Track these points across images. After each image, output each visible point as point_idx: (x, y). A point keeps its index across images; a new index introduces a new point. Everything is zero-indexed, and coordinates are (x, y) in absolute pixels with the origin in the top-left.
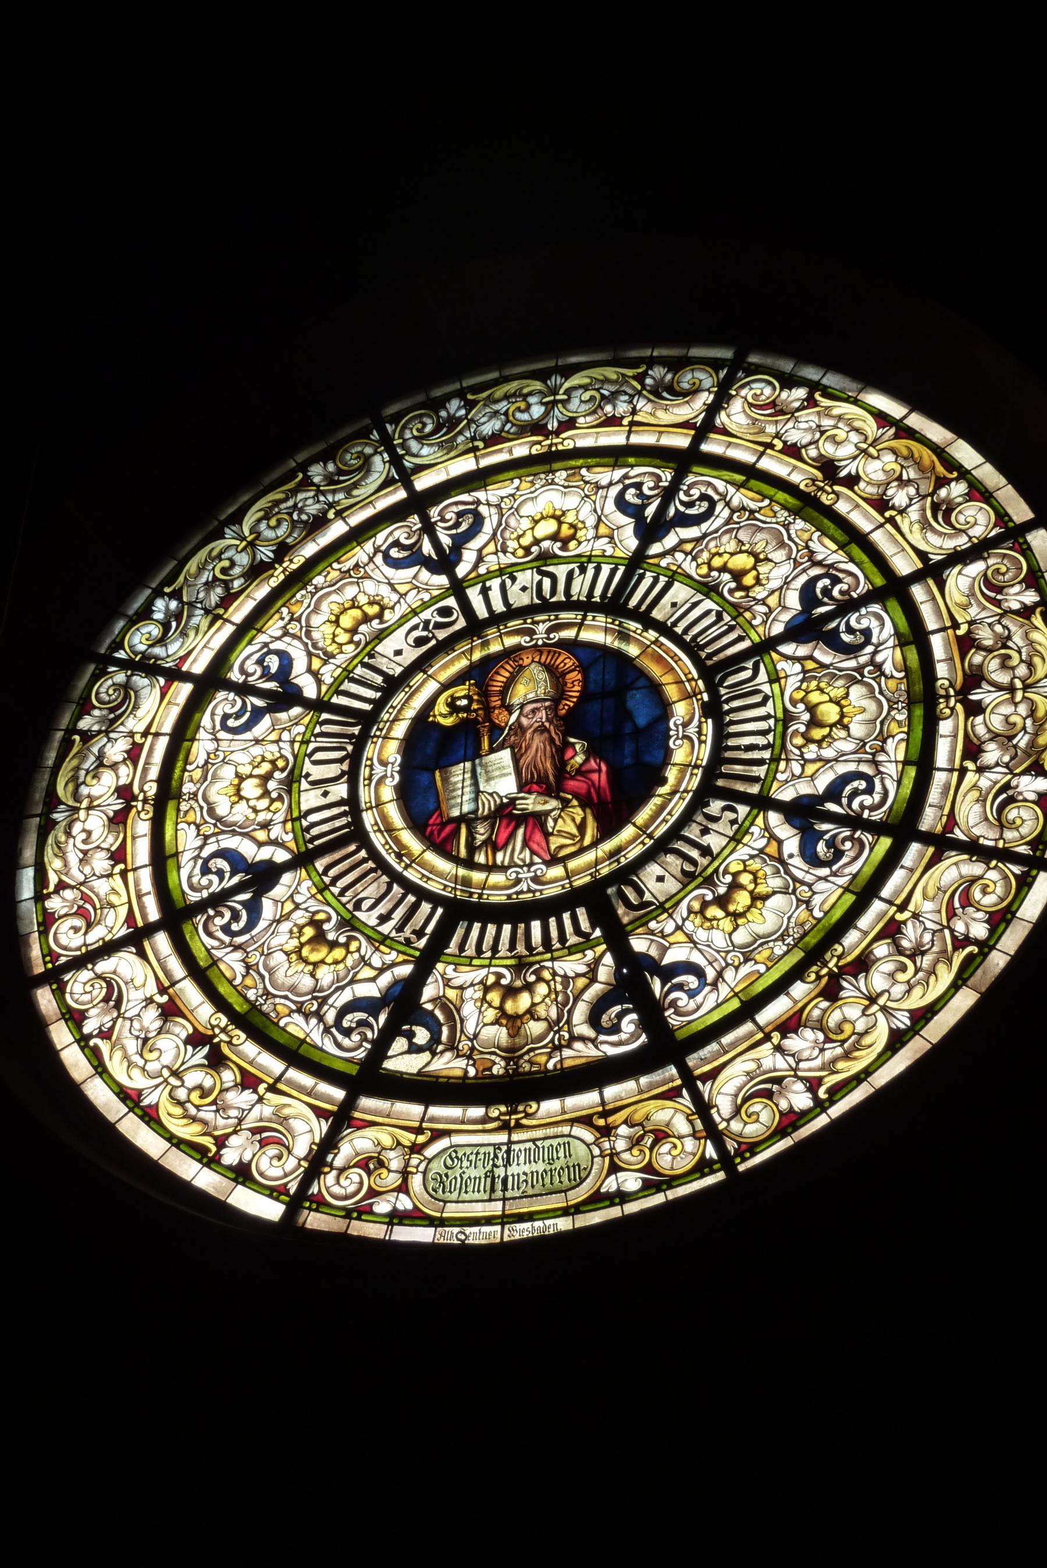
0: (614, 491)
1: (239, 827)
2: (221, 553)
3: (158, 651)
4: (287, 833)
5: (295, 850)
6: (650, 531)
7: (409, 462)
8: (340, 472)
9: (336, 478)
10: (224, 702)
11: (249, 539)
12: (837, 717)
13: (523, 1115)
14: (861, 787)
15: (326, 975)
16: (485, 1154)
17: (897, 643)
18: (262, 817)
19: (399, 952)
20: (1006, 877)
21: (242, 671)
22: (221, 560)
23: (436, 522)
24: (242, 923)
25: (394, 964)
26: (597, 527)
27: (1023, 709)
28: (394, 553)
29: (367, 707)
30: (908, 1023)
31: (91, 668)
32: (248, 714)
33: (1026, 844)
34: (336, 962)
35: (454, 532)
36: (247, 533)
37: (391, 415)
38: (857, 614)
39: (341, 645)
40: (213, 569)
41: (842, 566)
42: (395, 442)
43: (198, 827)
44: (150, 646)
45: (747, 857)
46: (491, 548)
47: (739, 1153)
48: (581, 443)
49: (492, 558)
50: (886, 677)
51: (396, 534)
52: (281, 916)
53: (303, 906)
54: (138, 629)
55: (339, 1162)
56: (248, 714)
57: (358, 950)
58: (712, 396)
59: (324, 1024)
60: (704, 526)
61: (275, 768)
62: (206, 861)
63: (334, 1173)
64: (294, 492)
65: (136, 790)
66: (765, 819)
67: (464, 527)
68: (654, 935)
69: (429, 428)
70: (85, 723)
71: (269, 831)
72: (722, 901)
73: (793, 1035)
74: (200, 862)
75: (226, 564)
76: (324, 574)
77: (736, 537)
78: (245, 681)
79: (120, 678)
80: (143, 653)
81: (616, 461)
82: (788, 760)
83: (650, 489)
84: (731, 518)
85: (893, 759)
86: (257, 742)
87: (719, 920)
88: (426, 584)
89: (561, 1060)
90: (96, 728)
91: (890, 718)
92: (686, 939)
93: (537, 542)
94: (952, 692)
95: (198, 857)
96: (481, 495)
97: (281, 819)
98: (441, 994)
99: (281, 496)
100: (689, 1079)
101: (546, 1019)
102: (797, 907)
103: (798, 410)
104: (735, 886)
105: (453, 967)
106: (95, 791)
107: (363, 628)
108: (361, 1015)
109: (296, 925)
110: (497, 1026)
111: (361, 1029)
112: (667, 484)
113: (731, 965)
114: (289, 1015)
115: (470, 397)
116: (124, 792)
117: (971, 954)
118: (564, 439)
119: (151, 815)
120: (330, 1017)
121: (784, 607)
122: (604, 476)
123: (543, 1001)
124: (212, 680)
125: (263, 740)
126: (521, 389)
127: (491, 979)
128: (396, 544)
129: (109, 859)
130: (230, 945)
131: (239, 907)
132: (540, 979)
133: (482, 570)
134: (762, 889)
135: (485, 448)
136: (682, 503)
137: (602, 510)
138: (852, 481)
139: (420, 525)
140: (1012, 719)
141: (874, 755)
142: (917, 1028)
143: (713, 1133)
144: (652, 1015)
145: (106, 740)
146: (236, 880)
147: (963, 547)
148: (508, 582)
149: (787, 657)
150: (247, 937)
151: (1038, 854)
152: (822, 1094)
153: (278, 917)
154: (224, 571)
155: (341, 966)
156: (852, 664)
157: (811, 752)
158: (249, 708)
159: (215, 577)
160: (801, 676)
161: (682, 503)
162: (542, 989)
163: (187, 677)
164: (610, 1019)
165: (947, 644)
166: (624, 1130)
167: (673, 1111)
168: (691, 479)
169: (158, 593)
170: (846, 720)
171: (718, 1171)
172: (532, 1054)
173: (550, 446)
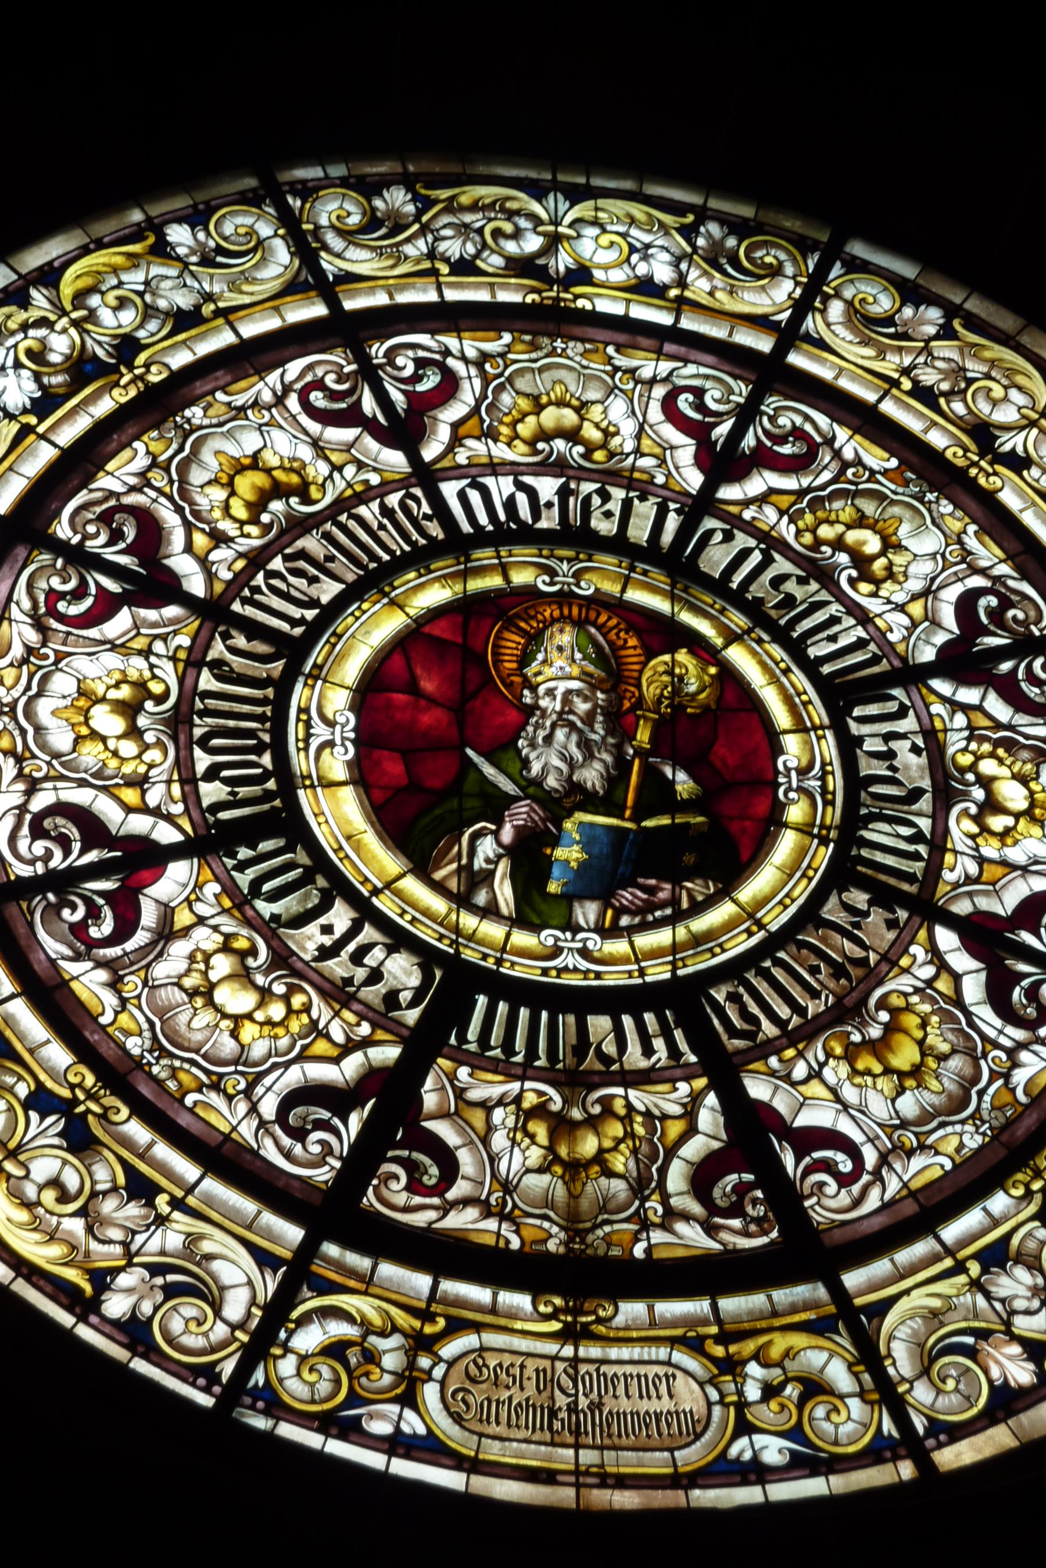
0: (977, 581)
2: (518, 213)
3: (335, 242)
4: (914, 957)
7: (812, 323)
9: (723, 261)
10: (331, 364)
11: (560, 229)
12: (906, 1067)
13: (969, 454)
14: (320, 395)
15: (91, 754)
16: (537, 1371)
17: (101, 474)
18: (227, 526)
19: (927, 706)
21: (391, 354)
22: (508, 219)
23: (340, 1158)
24: (75, 610)
25: (944, 700)
26: (914, 598)
28: (684, 402)
29: (466, 528)
30: (551, 197)
31: (251, 182)
32: (817, 1155)
33: (928, 1417)
35: (769, 444)
36: (567, 220)
37: (855, 258)
39: (517, 436)
40: (490, 220)
41: (27, 604)
43: (154, 464)
44: (332, 226)
45: (643, 1109)
47: (256, 1393)
49: (770, 514)
51: (401, 1199)
52: (123, 645)
53: (153, 659)
56: (817, 1155)
57: (965, 750)
59: (27, 802)
60: (1021, 719)
65: (141, 359)
67: (786, 449)
69: (355, 220)
71: (216, 547)
72: (562, 1127)
74: (112, 503)
75: (508, 227)
76: (588, 346)
77: (74, 751)
78: (380, 366)
79: (922, 1393)
80: (318, 228)
81: (1017, 555)
82: (800, 1054)
85: (906, 1178)
86: (315, 443)
87: (534, 1143)
88: (677, 468)
90: (181, 251)
91: (958, 1128)
95: (118, 495)
97: (241, 549)
98: (172, 904)
101: (242, 1046)
102: (627, 1220)
105: (889, 635)
106: (106, 316)
107: (560, 444)
108: (74, 833)
109: (123, 672)
110: (186, 999)
112: (1037, 633)
113: (634, 379)
115: (956, 324)
116: (127, 346)
118: (995, 474)
120: (41, 801)
121: (136, 626)
122: (987, 553)
123: (838, 522)
125: (322, 449)
126: (20, 1226)
127: (241, 944)
128: (414, 1186)
129: (31, 399)
131: (93, 590)
132: (286, 998)
133: (748, 515)
134: (524, 404)
135: (909, 393)
138: (40, 1101)
142: (549, 185)
144: (786, 1200)
146: (124, 560)
151: (930, 1443)
152: (690, 218)
153: (118, 642)
154: (497, 233)
155: (113, 763)
157: (835, 1072)
158: (807, 1160)
159: (480, 231)
161: (1029, 668)
162: (826, 532)
164: (304, 1119)
166: (753, 1369)
168: (322, 1175)
169: (408, 182)
172: (186, 1066)
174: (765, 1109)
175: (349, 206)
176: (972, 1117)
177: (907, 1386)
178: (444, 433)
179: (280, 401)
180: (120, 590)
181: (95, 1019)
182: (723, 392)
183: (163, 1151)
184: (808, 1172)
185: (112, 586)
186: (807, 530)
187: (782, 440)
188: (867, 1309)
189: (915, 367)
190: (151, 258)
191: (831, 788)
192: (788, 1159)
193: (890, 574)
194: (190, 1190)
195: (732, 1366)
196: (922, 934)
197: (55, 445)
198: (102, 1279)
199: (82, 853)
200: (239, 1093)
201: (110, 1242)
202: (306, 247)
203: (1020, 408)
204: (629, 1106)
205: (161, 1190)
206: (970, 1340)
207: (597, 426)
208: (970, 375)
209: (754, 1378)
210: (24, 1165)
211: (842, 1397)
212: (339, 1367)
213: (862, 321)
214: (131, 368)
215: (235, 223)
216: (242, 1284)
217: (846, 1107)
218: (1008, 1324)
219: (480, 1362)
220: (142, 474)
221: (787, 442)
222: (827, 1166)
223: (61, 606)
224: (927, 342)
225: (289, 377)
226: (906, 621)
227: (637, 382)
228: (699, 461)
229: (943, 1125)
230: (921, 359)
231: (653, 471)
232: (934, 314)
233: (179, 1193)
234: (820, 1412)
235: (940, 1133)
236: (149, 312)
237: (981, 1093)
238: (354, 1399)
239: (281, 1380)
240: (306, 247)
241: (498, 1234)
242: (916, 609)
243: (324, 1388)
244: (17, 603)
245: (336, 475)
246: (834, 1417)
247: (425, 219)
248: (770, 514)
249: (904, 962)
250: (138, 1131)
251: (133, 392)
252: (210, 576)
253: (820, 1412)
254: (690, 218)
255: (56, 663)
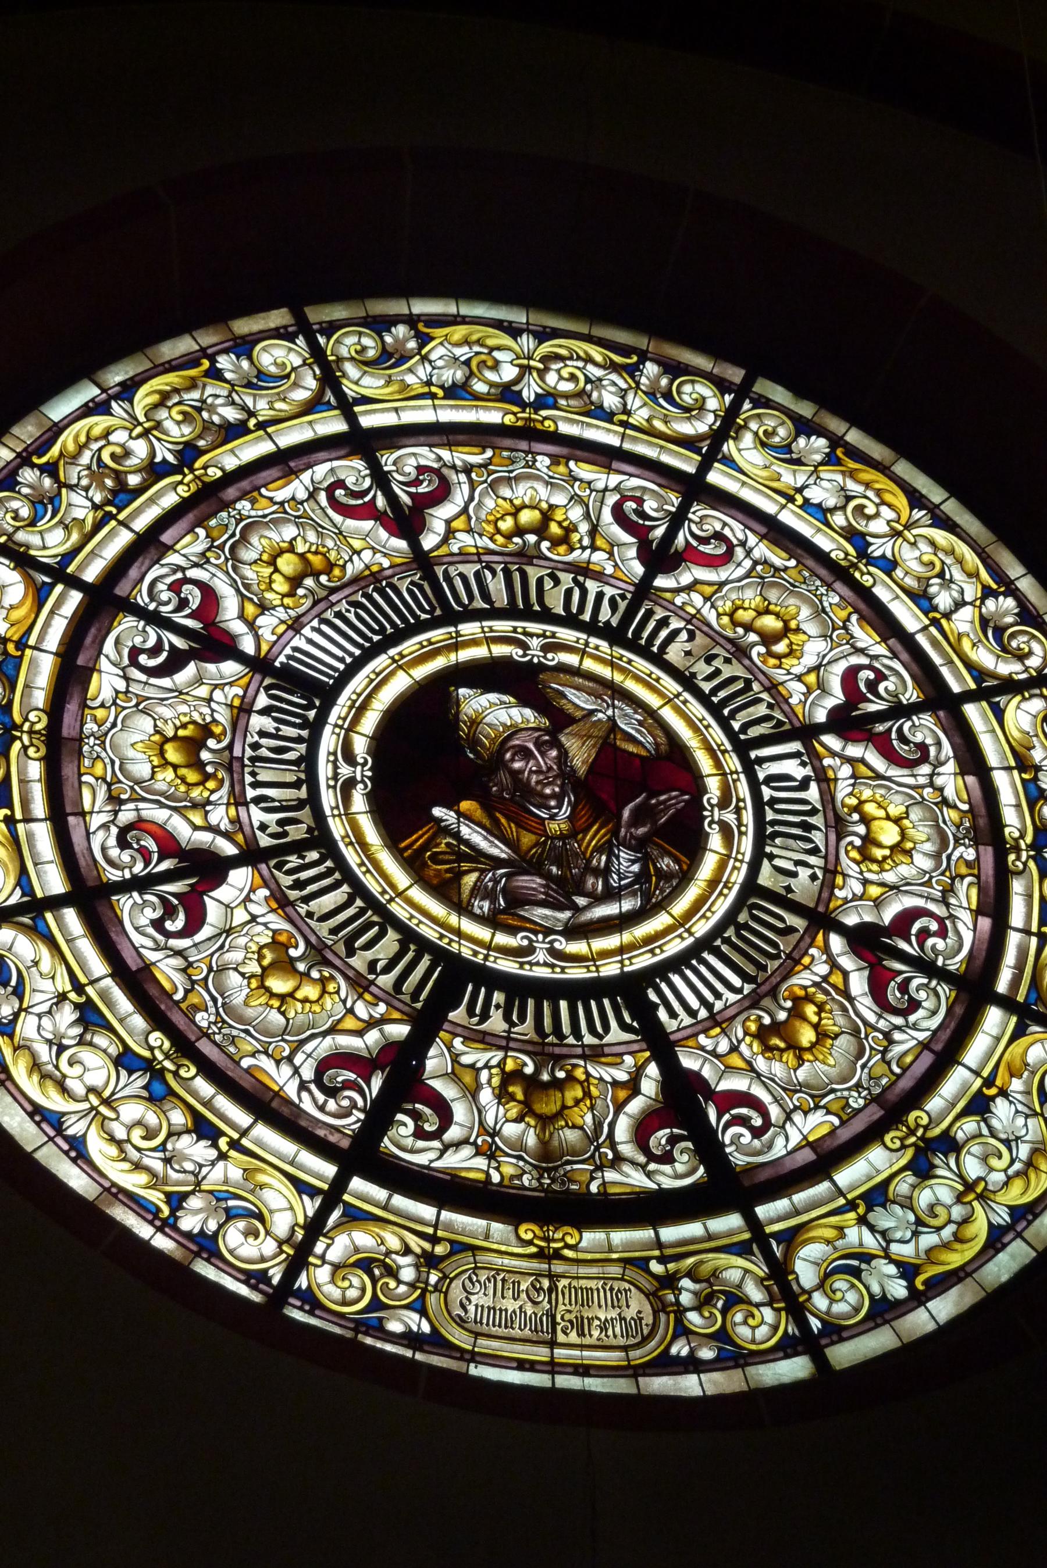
1: (243, 584)
3: (756, 1295)
4: (273, 633)
5: (263, 654)
6: (848, 722)
8: (668, 396)
14: (343, 492)
20: (775, 1328)
24: (152, 663)
27: (957, 1212)
34: (183, 780)
35: (694, 543)
38: (925, 981)
41: (960, 926)
42: (291, 1252)
44: (352, 359)
46: (708, 590)
47: (299, 1294)
48: (879, 592)
49: (697, 599)
50: (883, 1059)
54: (360, 334)
55: (1017, 667)
58: (1024, 676)
61: (328, 571)
62: (904, 1013)
63: (327, 1268)
64: (614, 367)
66: (647, 1061)
68: (449, 1050)
69: (371, 353)
70: (224, 362)
71: (262, 614)
73: (232, 420)
74: (179, 575)
83: (886, 689)
84: (923, 787)
89: (604, 1184)
92: (598, 537)
93: (748, 628)
94: (919, 1133)
95: (183, 570)
96: (291, 1090)
97: (806, 974)
99: (599, 358)
100: (333, 1195)
103: (821, 464)
104: (557, 1085)
111: (138, 856)
114: (97, 779)
115: (839, 452)
117: (426, 326)
118: (869, 573)
119: (186, 495)
124: (363, 443)
130: (123, 669)
131: (913, 938)
136: (900, 730)
137: (829, 663)
138: (889, 565)
139: (673, 509)
140: (939, 1210)
141: (796, 1108)
143: (299, 1259)
144: (709, 1148)
145: (226, 393)
146: (190, 623)
147: (7, 562)
148: (684, 636)
149: (257, 638)
150: (143, 677)
152: (206, 364)
156: (871, 1018)
160: (818, 979)
163: (351, 418)
165: (965, 1087)
166: (686, 1283)
167: (286, 1205)
170: (808, 1056)
171: (261, 1292)
173: (167, 1056)
174: (696, 1077)
175: (367, 341)
176: (241, 520)
177: (806, 1296)
178: (439, 527)
179: (312, 495)
180: (186, 647)
181: (169, 996)
182: (658, 503)
183: (223, 1103)
184: (728, 1125)
185: (180, 643)
186: (725, 614)
187: (704, 541)
188: (777, 1236)
189: (807, 486)
190: (918, 1262)
191: (330, 765)
192: (712, 1114)
193: (791, 653)
194: (244, 1133)
195: (670, 1281)
196: (265, 648)
197: (132, 530)
198: (176, 1201)
199: (890, 730)
200: (283, 1058)
201: (185, 1172)
202: (330, 377)
203: (117, 1119)
204: (588, 1074)
205: (223, 1134)
206: (855, 1263)
207: (560, 523)
208: (161, 1155)
209: (687, 1290)
210: (114, 1110)
211: (352, 359)
212: (366, 1278)
213: (257, 1218)
214: (192, 470)
215: (272, 355)
216: (286, 1210)
217: (759, 1075)
218: (886, 1250)
219: (475, 1278)
220: (203, 554)
221: (709, 544)
222: (742, 1121)
223: (143, 659)
224: (816, 467)
225: (318, 477)
226: (804, 689)
227: (592, 491)
228: (641, 557)
229: (265, 516)
230: (811, 481)
231: (603, 563)
232: (821, 443)
233: (235, 1136)
234: (739, 1317)
235: (267, 512)
236: (908, 1204)
237: (233, 535)
238: (376, 1304)
239: (319, 1286)
240: (330, 377)
241: (487, 1173)
242: (812, 678)
243: (687, 388)
244: (107, 657)
245: (355, 558)
246: (751, 1321)
247: (423, 352)
248: (697, 599)
249: (806, 960)
250: (205, 1088)
251: (193, 488)
252: (826, 949)
253: (739, 1317)
254: (635, 359)
255: (931, 878)
